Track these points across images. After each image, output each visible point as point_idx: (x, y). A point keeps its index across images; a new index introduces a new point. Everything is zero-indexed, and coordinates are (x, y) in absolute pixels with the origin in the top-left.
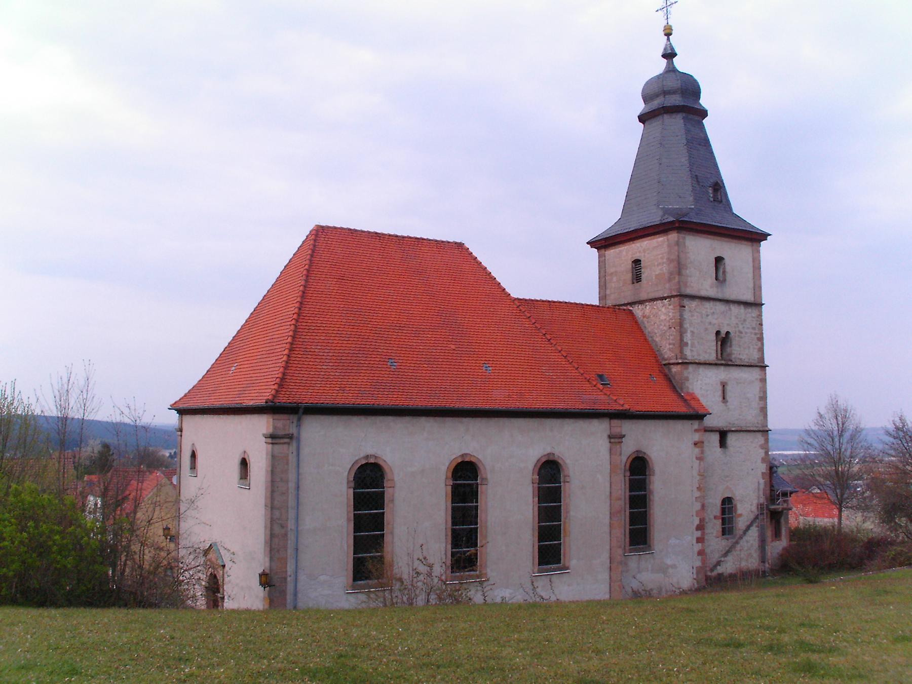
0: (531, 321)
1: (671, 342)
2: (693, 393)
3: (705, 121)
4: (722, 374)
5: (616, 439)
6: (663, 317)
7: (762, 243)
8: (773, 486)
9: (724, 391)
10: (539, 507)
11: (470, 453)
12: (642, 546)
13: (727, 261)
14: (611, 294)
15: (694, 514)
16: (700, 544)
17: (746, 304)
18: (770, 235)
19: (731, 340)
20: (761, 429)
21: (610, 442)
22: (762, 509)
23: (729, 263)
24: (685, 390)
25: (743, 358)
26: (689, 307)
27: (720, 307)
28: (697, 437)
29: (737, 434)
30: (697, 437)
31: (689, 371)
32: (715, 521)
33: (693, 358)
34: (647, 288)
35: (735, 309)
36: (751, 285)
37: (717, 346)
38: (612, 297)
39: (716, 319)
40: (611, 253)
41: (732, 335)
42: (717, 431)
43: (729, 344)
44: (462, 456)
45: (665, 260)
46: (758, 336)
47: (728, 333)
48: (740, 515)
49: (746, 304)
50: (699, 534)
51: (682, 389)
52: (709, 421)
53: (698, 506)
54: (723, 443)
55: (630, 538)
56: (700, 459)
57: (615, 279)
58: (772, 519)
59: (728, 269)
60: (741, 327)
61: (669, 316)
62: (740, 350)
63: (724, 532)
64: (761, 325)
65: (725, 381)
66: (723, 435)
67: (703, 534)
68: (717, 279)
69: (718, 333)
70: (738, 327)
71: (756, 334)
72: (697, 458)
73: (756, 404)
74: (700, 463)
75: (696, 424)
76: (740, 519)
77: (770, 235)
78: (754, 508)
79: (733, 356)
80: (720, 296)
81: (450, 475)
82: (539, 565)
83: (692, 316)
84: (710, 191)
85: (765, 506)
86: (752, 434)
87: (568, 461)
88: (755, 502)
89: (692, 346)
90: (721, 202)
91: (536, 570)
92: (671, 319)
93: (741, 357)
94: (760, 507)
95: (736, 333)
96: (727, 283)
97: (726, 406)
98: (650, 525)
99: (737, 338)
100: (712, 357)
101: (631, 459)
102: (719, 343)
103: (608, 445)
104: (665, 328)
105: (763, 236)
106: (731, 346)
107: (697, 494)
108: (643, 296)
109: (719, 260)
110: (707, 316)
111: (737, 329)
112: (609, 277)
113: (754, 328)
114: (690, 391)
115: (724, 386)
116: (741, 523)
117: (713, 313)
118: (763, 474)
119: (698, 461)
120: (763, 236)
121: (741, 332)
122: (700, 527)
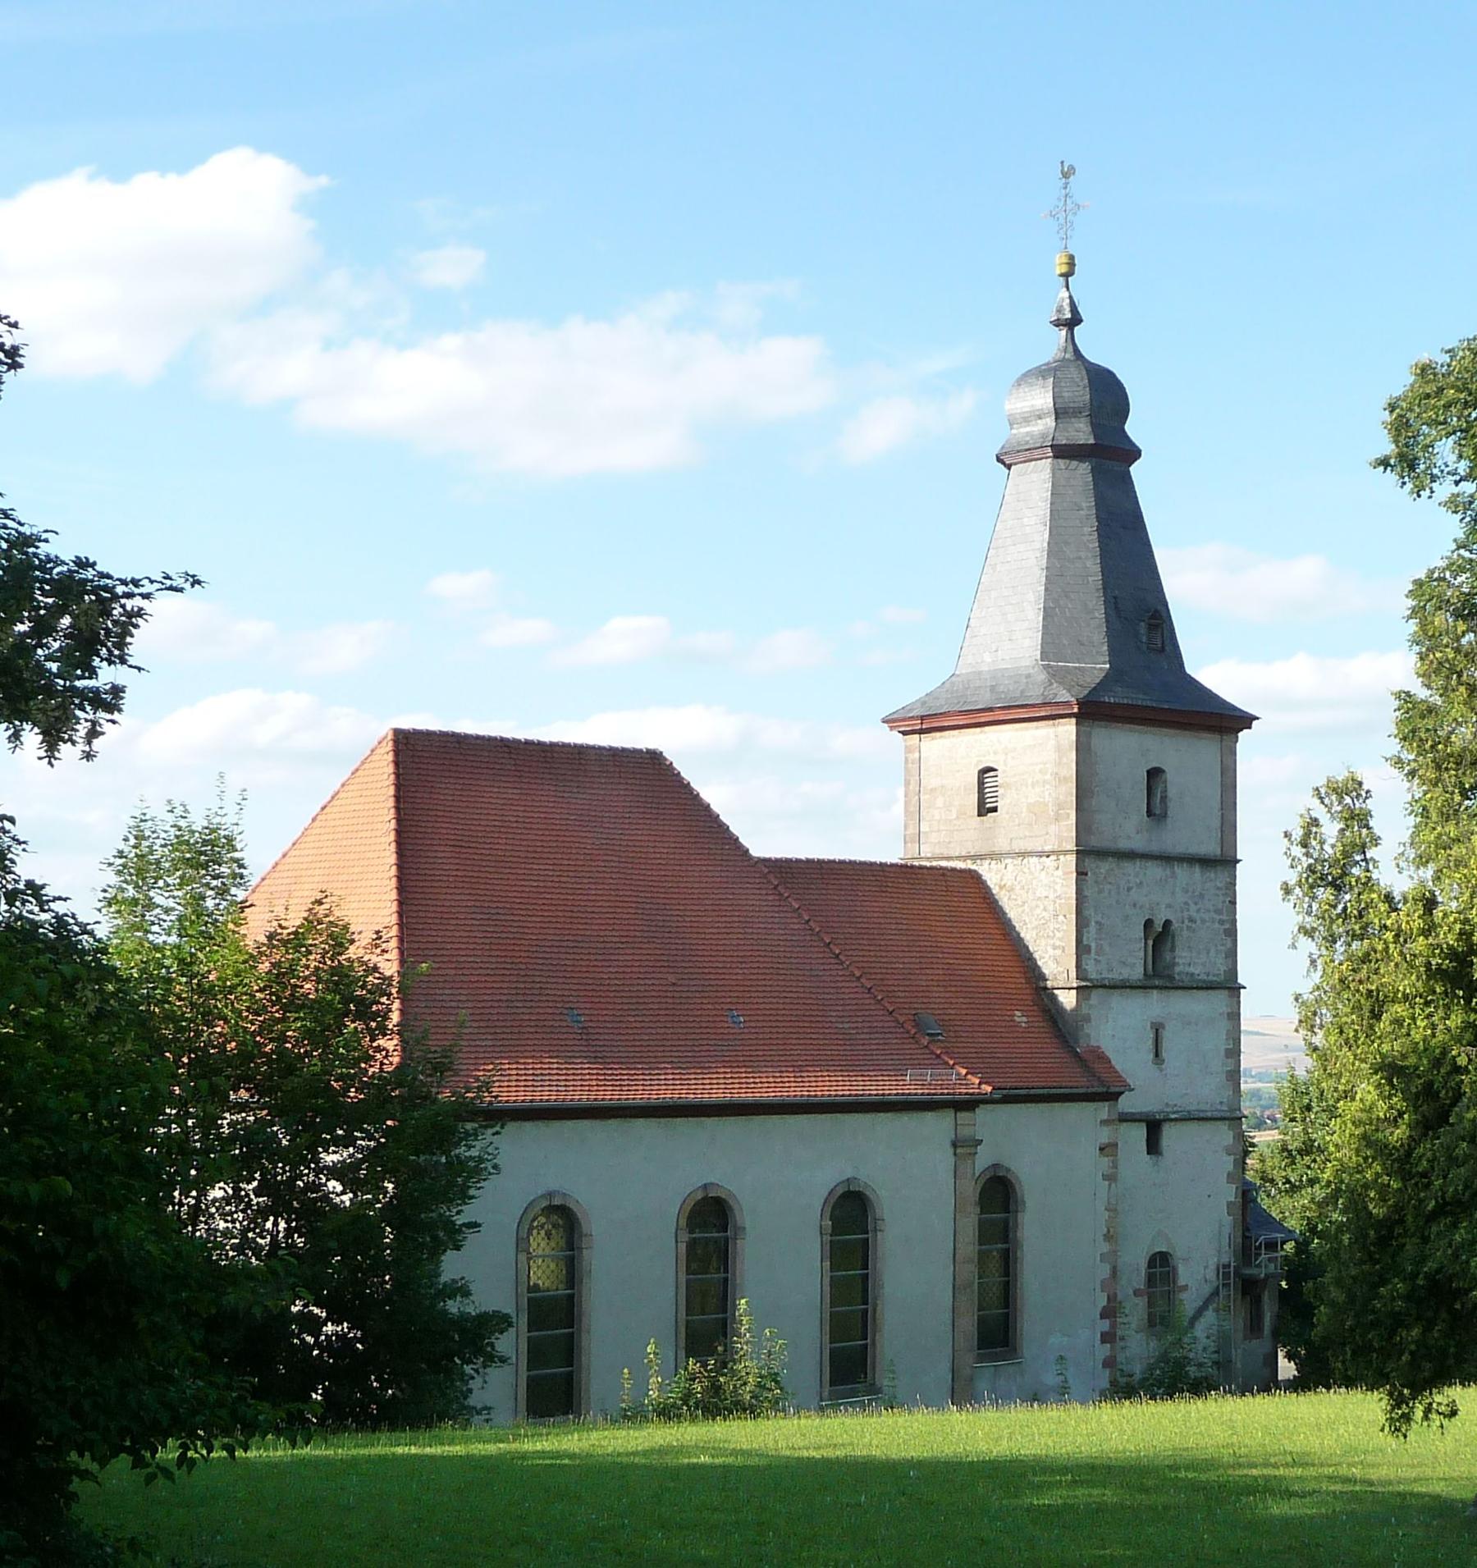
0: (800, 916)
1: (1058, 943)
2: (1099, 1047)
3: (1135, 470)
4: (1155, 1005)
5: (964, 1146)
6: (1041, 892)
7: (1240, 734)
8: (1248, 1230)
9: (1157, 1040)
10: (831, 1277)
11: (716, 1182)
12: (998, 1349)
13: (1169, 775)
14: (932, 832)
15: (1098, 1287)
16: (1108, 1345)
17: (1206, 862)
18: (1258, 718)
19: (1173, 937)
20: (1228, 1115)
21: (955, 1154)
22: (1226, 1275)
23: (1175, 783)
24: (1082, 1042)
25: (1197, 972)
26: (1094, 873)
27: (1155, 871)
28: (1105, 1135)
29: (1179, 1125)
30: (1105, 1135)
31: (1091, 1002)
32: (1137, 1300)
33: (1099, 977)
34: (1006, 828)
35: (1182, 872)
36: (1217, 823)
37: (1146, 951)
38: (934, 838)
39: (1146, 896)
40: (935, 746)
41: (1175, 925)
42: (1140, 1121)
43: (1169, 945)
44: (705, 1187)
45: (1048, 777)
46: (1227, 926)
47: (1167, 923)
48: (1185, 1288)
49: (1206, 862)
50: (1105, 1325)
51: (1077, 1041)
52: (1126, 1104)
53: (1105, 1271)
54: (1153, 1146)
55: (831, 1366)
56: (1111, 1178)
57: (940, 802)
58: (1244, 1294)
59: (1172, 792)
60: (1193, 908)
61: (1055, 891)
62: (1187, 960)
63: (1151, 1323)
64: (1233, 903)
65: (1159, 1020)
66: (1154, 1127)
67: (1113, 1326)
68: (1150, 813)
69: (1148, 924)
70: (1188, 910)
71: (1222, 922)
72: (1105, 1177)
73: (1218, 1064)
74: (1110, 1185)
75: (1103, 1110)
76: (1183, 1296)
77: (1258, 718)
78: (1211, 1274)
79: (1177, 969)
80: (1154, 848)
81: (683, 1222)
82: (831, 1386)
83: (1100, 891)
84: (1143, 628)
85: (1232, 1269)
86: (1208, 1125)
87: (882, 1193)
88: (1213, 1262)
89: (1097, 954)
90: (1163, 649)
91: (826, 1394)
92: (1059, 897)
93: (1192, 969)
94: (1223, 1270)
95: (1183, 922)
96: (1169, 820)
97: (1161, 1071)
98: (1015, 1309)
99: (1185, 933)
100: (1136, 973)
101: (983, 1181)
102: (1150, 943)
103: (952, 1159)
104: (1044, 914)
105: (1245, 721)
106: (1173, 949)
107: (1105, 1247)
108: (1002, 845)
109: (1154, 774)
110: (1129, 889)
111: (1186, 914)
112: (927, 796)
113: (1218, 912)
114: (1093, 1043)
115: (1158, 1030)
116: (1189, 1301)
117: (1141, 883)
118: (1229, 1204)
119: (1107, 1183)
120: (1245, 721)
121: (1191, 920)
122: (1108, 1313)
